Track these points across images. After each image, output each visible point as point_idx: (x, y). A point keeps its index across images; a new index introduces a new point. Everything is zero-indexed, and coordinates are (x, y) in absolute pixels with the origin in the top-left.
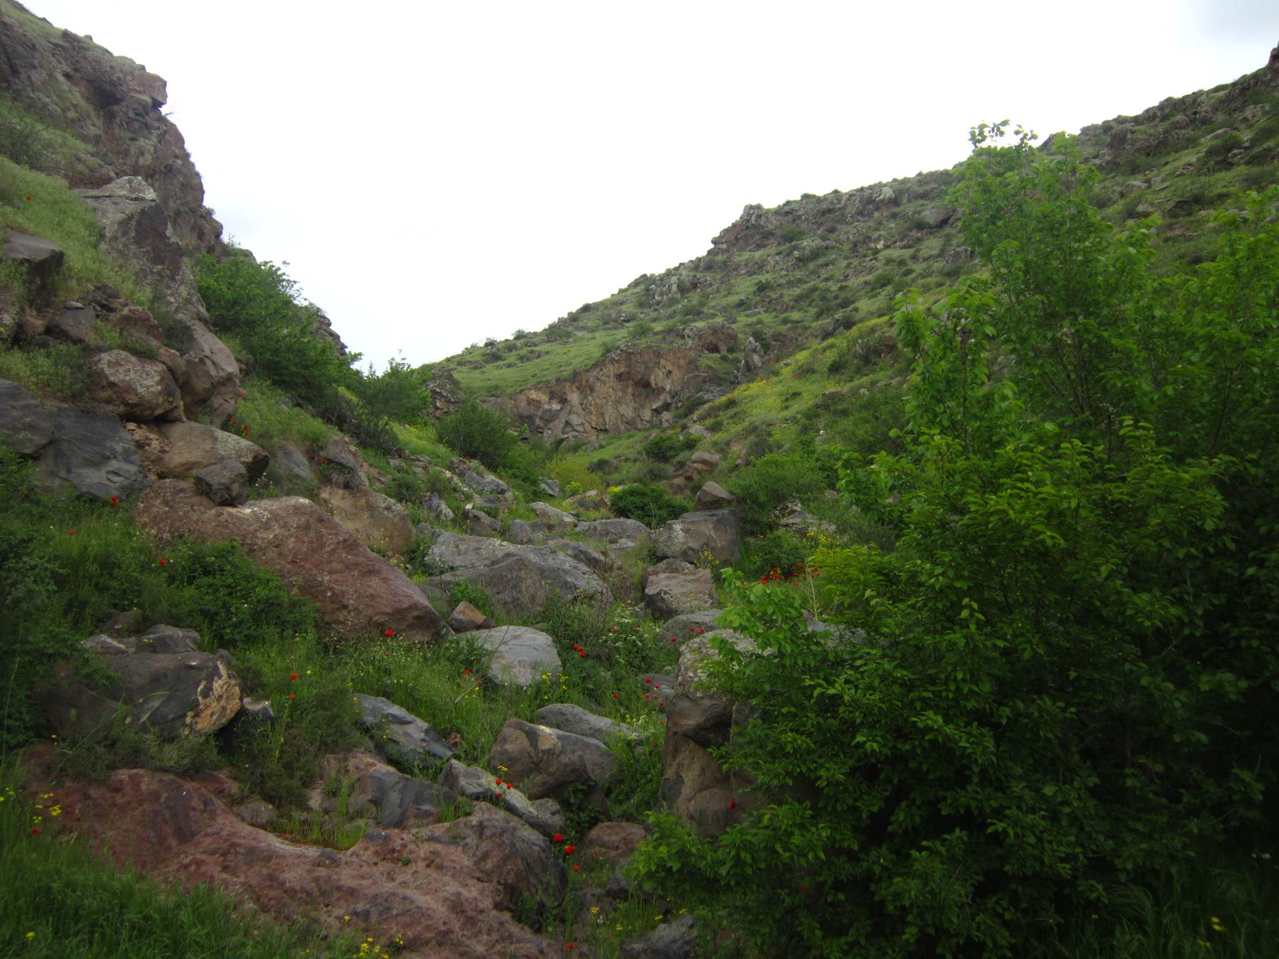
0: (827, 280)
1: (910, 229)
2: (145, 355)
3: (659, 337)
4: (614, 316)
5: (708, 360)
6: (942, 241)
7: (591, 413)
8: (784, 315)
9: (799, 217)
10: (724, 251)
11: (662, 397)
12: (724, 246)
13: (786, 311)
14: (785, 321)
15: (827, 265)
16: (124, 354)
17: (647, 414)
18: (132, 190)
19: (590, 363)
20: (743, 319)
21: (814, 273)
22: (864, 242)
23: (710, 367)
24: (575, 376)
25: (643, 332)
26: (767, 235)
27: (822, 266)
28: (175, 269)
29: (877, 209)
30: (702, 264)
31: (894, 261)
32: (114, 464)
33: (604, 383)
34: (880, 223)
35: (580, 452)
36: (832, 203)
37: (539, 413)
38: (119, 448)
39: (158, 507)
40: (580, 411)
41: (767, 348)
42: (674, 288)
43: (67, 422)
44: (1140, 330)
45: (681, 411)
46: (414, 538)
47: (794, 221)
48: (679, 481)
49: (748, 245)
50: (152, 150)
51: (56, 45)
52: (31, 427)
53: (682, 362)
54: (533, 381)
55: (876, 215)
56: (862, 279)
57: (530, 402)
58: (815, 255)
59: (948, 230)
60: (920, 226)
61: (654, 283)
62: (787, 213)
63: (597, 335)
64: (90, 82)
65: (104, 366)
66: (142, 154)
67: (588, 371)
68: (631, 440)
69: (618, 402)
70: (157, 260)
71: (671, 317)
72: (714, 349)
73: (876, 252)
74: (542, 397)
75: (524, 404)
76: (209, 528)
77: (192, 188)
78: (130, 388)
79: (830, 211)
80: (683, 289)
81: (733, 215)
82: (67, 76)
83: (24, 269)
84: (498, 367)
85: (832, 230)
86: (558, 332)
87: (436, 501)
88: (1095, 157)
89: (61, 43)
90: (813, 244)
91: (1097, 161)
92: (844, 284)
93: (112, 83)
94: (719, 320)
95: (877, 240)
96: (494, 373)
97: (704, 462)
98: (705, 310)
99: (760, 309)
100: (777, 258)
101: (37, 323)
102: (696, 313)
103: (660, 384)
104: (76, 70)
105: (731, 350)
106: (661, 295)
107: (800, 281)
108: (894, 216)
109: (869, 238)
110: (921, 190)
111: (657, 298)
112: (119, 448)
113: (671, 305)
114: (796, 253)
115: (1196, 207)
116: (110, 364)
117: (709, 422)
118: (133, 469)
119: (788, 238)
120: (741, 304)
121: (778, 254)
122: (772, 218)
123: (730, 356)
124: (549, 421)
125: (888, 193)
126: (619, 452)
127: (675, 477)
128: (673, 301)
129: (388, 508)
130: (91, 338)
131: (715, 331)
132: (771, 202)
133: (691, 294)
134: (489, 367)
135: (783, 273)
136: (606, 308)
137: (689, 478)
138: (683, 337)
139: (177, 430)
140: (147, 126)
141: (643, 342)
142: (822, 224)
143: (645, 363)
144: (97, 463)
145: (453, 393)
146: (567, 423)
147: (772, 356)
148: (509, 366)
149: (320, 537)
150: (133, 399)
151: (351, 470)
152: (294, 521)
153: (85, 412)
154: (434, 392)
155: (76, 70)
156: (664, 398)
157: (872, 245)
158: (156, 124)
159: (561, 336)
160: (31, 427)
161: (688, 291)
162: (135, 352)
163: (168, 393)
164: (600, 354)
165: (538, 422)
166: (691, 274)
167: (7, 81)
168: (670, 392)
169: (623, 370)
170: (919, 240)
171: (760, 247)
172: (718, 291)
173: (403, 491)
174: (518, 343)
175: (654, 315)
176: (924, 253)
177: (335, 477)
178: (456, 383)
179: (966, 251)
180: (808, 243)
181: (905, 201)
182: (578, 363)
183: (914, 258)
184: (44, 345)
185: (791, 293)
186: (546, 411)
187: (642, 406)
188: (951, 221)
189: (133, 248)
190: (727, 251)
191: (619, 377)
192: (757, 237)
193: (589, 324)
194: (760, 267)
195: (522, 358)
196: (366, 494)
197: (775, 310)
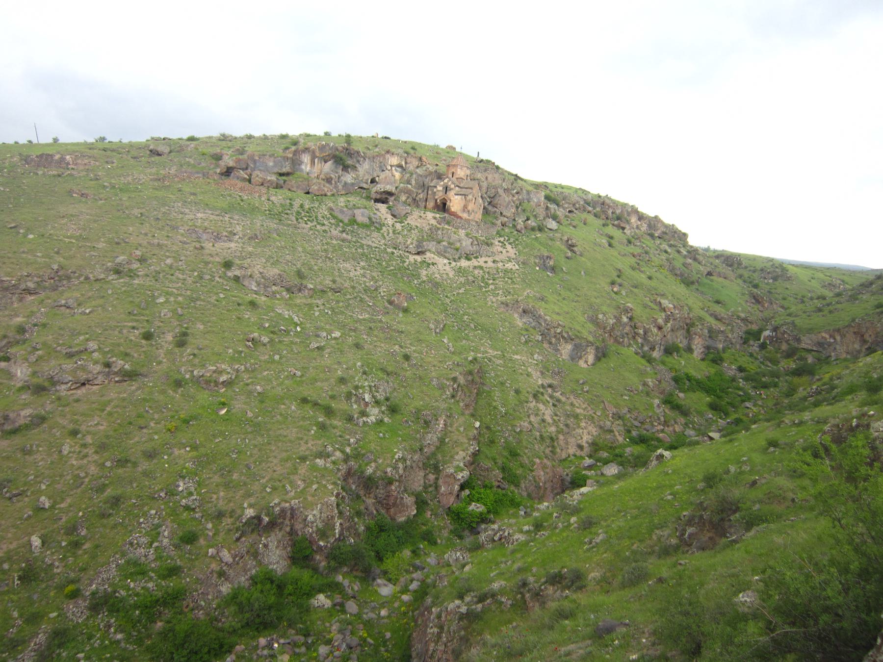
24: (838, 331)
57: (823, 337)
74: (827, 336)
84: (818, 316)
145: (792, 331)
148: (823, 316)
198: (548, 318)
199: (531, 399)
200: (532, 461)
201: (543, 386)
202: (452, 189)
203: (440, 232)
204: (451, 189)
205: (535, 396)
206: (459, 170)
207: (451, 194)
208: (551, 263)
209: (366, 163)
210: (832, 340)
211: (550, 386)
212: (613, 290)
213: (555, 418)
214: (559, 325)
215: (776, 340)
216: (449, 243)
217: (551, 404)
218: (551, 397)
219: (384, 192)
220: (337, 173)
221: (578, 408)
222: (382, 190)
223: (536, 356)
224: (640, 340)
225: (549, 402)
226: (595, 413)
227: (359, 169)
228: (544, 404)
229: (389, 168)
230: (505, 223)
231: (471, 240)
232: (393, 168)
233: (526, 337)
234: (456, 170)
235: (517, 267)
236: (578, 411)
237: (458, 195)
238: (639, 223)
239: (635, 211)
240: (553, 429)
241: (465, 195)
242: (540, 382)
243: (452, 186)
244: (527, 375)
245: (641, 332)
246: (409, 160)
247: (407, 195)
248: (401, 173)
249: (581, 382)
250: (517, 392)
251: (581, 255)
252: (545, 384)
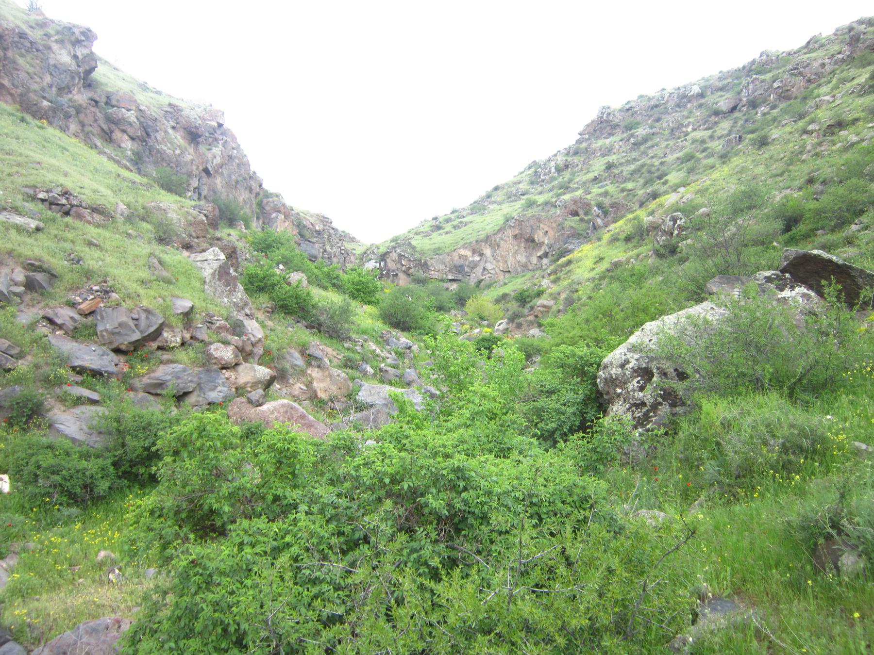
0: (652, 157)
1: (710, 116)
2: (226, 343)
3: (540, 208)
4: (514, 192)
5: (572, 222)
6: (731, 122)
7: (499, 261)
8: (622, 186)
9: (636, 112)
10: (586, 140)
11: (543, 248)
12: (587, 136)
13: (625, 182)
14: (623, 190)
15: (653, 146)
16: (219, 344)
17: (534, 260)
18: (215, 255)
19: (497, 228)
20: (596, 190)
21: (644, 153)
22: (678, 128)
23: (572, 227)
24: (487, 239)
25: (531, 204)
26: (615, 126)
27: (649, 148)
28: (235, 286)
29: (689, 102)
30: (571, 151)
31: (697, 141)
32: (219, 388)
33: (506, 241)
34: (691, 112)
35: (492, 288)
36: (658, 100)
37: (467, 263)
38: (220, 382)
39: (236, 409)
40: (492, 260)
41: (606, 213)
42: (553, 170)
43: (202, 376)
44: (232, 505)
45: (556, 257)
46: (351, 388)
47: (632, 115)
48: (531, 318)
49: (602, 134)
50: (220, 153)
51: (166, 112)
52: (191, 381)
53: (554, 225)
54: (462, 243)
55: (689, 105)
56: (676, 156)
57: (460, 257)
58: (645, 140)
59: (737, 114)
60: (716, 113)
61: (540, 167)
62: (628, 110)
63: (503, 206)
64: (185, 129)
65: (212, 351)
66: (215, 157)
67: (495, 234)
68: (523, 279)
69: (516, 253)
70: (228, 285)
71: (551, 190)
72: (576, 214)
73: (687, 134)
74: (468, 253)
75: (457, 258)
76: (253, 416)
77: (244, 165)
78: (222, 359)
79: (656, 106)
80: (559, 170)
81: (592, 115)
82: (173, 128)
83: (181, 317)
84: (440, 234)
85: (658, 120)
86: (478, 208)
87: (364, 366)
88: (839, 53)
89: (169, 109)
90: (644, 133)
91: (840, 56)
92: (663, 160)
93: (196, 127)
94: (579, 193)
95: (687, 126)
96: (438, 239)
97: (544, 306)
98: (571, 185)
99: (608, 182)
100: (621, 143)
101: (187, 336)
102: (566, 188)
103: (541, 240)
104: (177, 123)
105: (586, 214)
106: (545, 175)
107: (635, 160)
108: (701, 106)
109: (682, 125)
110: (720, 84)
111: (542, 177)
112: (220, 382)
113: (551, 182)
114: (632, 140)
115: (837, 130)
116: (215, 350)
117: (552, 277)
118: (226, 389)
119: (629, 128)
120: (595, 179)
121: (621, 140)
122: (617, 115)
123: (586, 218)
124: (473, 268)
125: (696, 90)
126: (515, 287)
127: (528, 316)
128: (553, 179)
129: (338, 376)
130: (206, 339)
131: (575, 202)
132: (617, 103)
133: (564, 173)
134: (435, 234)
135: (624, 154)
136: (510, 187)
137: (536, 316)
138: (556, 207)
139: (241, 368)
140: (216, 140)
141: (530, 212)
142: (651, 116)
143: (531, 226)
144: (214, 389)
145: (412, 255)
146: (484, 269)
147: (610, 218)
148: (447, 233)
149: (292, 414)
150: (223, 362)
151: (320, 359)
152: (282, 410)
153: (208, 371)
154: (400, 255)
155: (177, 123)
156: (544, 249)
157: (684, 129)
158: (221, 137)
159: (480, 210)
160: (191, 381)
161: (563, 170)
162: (223, 343)
163: (236, 356)
164: (503, 222)
165: (466, 269)
166: (564, 158)
167: (145, 141)
168: (548, 245)
169: (517, 232)
170: (716, 123)
171: (611, 135)
172: (581, 170)
173: (348, 364)
174: (452, 216)
175: (540, 189)
176: (719, 132)
177: (313, 363)
178: (414, 248)
179: (736, 138)
180: (641, 132)
181: (709, 93)
182: (489, 229)
183: (711, 137)
184: (190, 345)
185: (628, 168)
186: (470, 262)
187: (531, 255)
188: (738, 108)
189: (218, 283)
190: (589, 139)
191: (515, 237)
192: (608, 128)
193: (499, 199)
194: (609, 151)
195: (455, 227)
196: (328, 369)
197: (617, 182)
210: (477, 258)
215: (388, 273)
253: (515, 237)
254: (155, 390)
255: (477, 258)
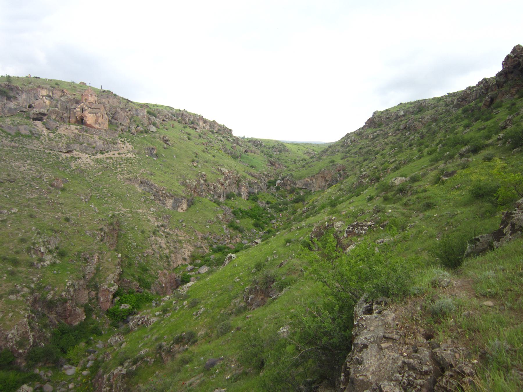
24: (314, 176)
57: (307, 181)
74: (309, 180)
198: (156, 185)
199: (152, 235)
200: (157, 272)
201: (158, 226)
202: (87, 110)
203: (81, 138)
204: (86, 110)
205: (154, 233)
206: (90, 97)
207: (86, 113)
208: (155, 152)
209: (24, 95)
210: (311, 182)
211: (162, 226)
212: (193, 165)
213: (167, 244)
214: (164, 188)
216: (88, 144)
217: (164, 236)
218: (164, 232)
219: (39, 113)
220: (3, 102)
221: (180, 236)
222: (38, 112)
223: (152, 209)
224: (212, 193)
225: (163, 236)
226: (191, 238)
227: (20, 98)
228: (160, 237)
229: (41, 97)
230: (124, 129)
231: (103, 141)
232: (44, 98)
233: (145, 198)
234: (88, 98)
235: (134, 156)
236: (181, 238)
237: (90, 113)
238: (204, 125)
239: (201, 118)
240: (167, 251)
241: (95, 113)
242: (156, 224)
243: (86, 108)
244: (148, 221)
245: (212, 188)
246: (54, 92)
247: (55, 115)
248: (50, 100)
249: (181, 221)
250: (143, 232)
251: (173, 146)
252: (159, 225)
253: (322, 177)
254: (220, 243)
255: (311, 182)
